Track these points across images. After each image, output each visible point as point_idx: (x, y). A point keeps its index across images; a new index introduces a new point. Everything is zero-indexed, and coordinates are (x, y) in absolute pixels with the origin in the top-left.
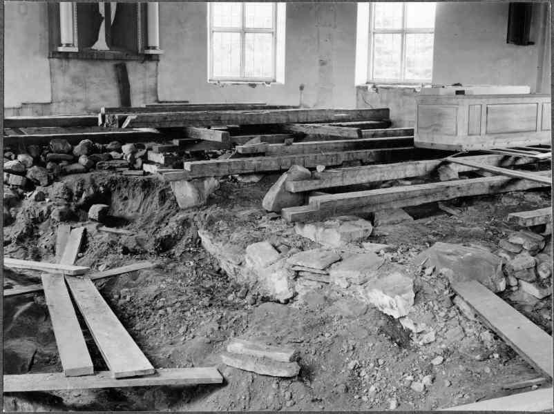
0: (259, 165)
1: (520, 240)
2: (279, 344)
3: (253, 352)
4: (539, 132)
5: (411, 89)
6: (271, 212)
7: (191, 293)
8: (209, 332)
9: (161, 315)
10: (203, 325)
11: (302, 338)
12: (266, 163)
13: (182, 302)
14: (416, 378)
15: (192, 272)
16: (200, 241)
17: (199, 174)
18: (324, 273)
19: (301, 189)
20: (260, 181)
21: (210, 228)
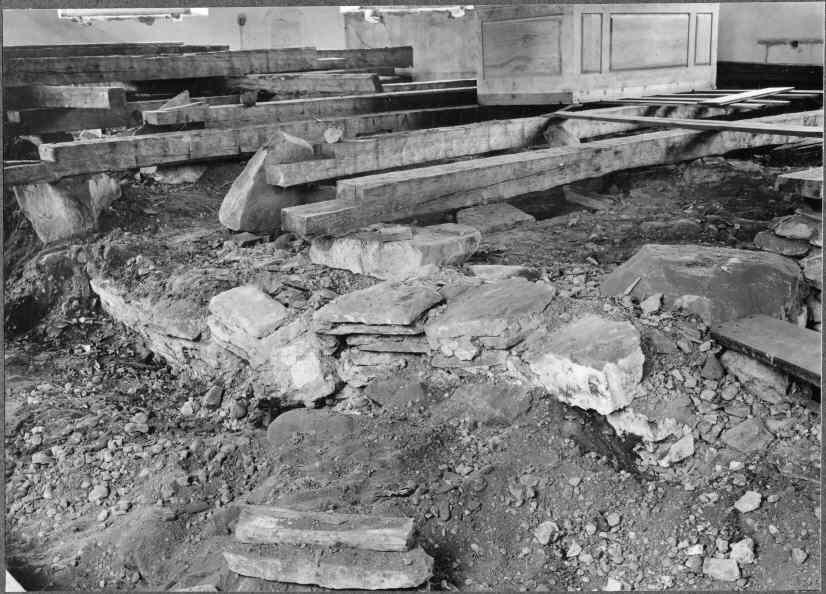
0: (197, 146)
1: (802, 230)
2: (355, 503)
3: (307, 536)
4: (691, 67)
5: (442, 12)
6: (239, 232)
7: (101, 407)
8: (167, 493)
9: (39, 465)
10: (147, 477)
11: (410, 484)
12: (211, 141)
13: (84, 431)
14: (709, 551)
15: (91, 365)
16: (99, 302)
17: (74, 166)
18: (411, 331)
19: (299, 181)
20: (200, 179)
21: (116, 273)
